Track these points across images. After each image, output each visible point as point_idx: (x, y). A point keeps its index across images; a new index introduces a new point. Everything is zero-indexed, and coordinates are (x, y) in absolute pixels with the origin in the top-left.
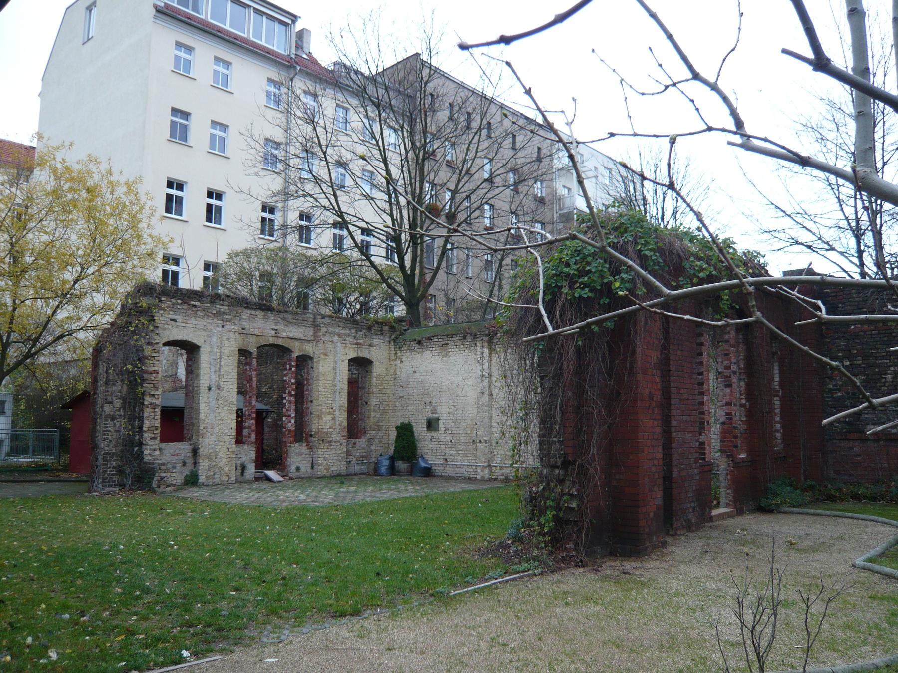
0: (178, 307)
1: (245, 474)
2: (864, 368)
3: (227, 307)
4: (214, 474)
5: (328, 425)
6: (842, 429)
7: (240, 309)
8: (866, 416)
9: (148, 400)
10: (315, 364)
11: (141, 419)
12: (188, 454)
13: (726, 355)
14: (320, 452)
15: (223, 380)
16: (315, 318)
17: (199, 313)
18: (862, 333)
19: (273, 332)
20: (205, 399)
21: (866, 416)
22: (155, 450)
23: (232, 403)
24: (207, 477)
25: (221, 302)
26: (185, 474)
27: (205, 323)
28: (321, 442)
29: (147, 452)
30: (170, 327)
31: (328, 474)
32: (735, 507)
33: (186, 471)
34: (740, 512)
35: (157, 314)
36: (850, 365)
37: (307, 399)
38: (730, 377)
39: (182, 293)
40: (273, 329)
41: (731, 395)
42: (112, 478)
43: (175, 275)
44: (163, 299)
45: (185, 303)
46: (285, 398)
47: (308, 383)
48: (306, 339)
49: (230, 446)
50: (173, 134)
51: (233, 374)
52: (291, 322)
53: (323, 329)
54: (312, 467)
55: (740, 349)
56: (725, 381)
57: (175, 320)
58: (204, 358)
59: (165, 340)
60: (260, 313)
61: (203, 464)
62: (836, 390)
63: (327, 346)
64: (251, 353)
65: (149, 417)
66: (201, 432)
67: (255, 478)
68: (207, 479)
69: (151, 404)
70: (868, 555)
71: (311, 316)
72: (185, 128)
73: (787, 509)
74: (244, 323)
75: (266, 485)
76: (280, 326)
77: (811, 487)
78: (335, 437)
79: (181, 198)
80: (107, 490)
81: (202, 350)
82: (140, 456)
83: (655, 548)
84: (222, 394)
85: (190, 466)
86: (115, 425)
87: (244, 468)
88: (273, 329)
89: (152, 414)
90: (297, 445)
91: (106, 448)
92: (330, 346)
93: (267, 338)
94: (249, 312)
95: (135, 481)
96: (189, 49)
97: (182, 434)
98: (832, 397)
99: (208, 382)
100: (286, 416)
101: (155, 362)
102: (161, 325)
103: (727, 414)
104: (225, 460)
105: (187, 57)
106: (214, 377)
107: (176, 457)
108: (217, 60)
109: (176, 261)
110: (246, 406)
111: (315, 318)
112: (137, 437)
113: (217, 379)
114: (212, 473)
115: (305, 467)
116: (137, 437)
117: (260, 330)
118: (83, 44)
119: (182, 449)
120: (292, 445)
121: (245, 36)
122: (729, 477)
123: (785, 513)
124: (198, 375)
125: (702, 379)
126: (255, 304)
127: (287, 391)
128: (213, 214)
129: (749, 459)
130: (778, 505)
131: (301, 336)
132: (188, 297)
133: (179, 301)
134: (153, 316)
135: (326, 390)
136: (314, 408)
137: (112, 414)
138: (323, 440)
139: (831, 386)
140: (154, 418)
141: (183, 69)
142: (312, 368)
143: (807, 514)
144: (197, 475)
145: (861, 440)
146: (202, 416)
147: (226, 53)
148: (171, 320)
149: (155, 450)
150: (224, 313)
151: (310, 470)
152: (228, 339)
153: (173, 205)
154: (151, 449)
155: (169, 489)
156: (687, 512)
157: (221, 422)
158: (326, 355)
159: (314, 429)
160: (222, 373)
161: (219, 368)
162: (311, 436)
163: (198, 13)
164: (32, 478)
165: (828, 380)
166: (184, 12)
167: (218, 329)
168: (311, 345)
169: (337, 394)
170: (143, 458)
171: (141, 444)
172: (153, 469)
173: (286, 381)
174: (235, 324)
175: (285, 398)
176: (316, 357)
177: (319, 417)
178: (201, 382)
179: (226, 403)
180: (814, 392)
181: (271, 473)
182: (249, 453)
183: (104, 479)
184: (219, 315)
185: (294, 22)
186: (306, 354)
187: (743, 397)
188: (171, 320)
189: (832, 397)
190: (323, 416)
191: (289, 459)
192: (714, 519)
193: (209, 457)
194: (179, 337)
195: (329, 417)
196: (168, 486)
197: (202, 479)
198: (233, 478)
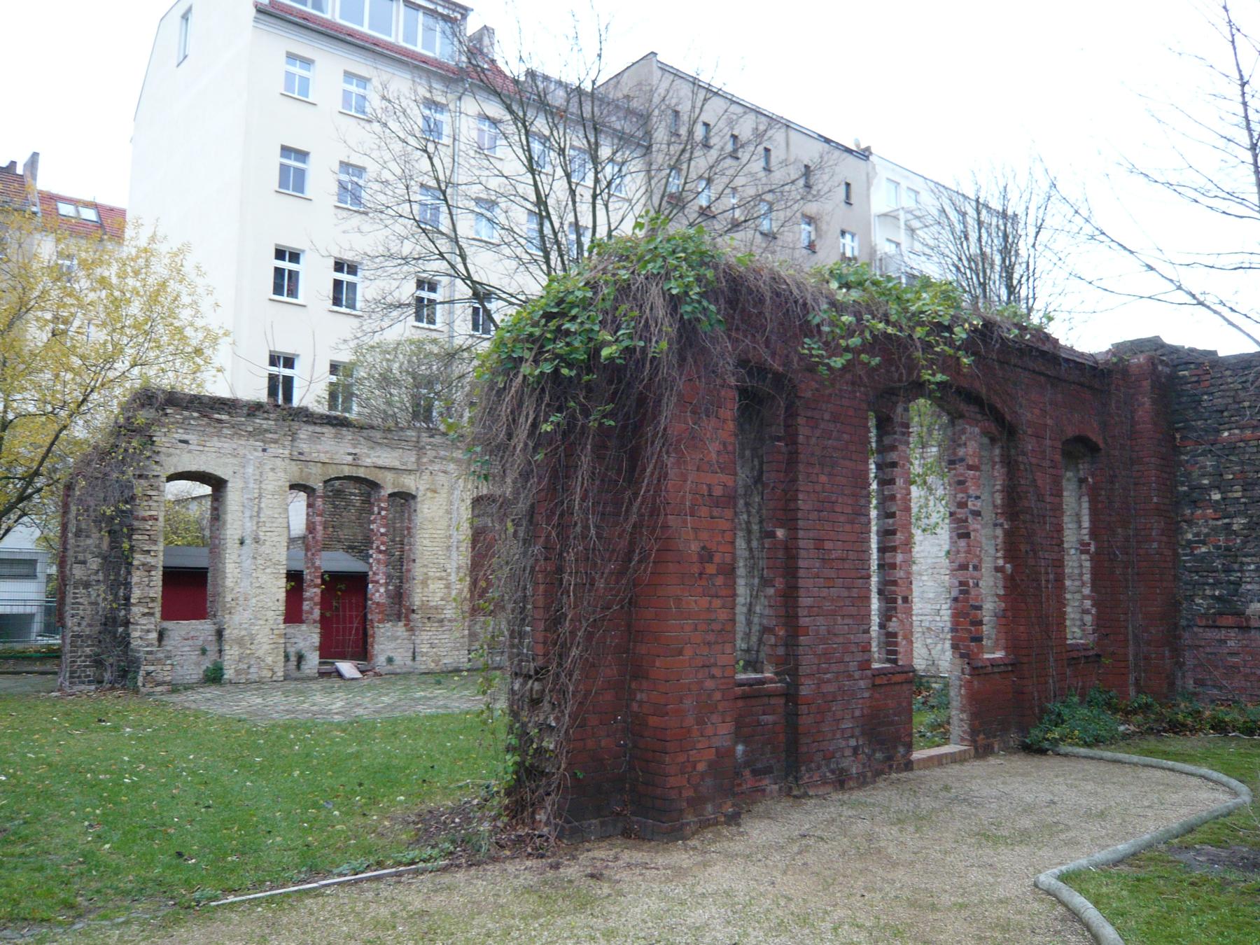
0: (192, 422)
1: (302, 667)
2: (1245, 504)
3: (273, 423)
4: (249, 668)
5: (439, 595)
6: (1208, 609)
7: (295, 425)
8: (1249, 587)
9: (138, 559)
10: (419, 506)
11: (127, 585)
12: (210, 638)
13: (961, 483)
14: (425, 636)
15: (264, 529)
16: (419, 437)
17: (225, 431)
18: (1242, 444)
20: (234, 557)
21: (1249, 587)
22: (148, 631)
23: (278, 563)
24: (238, 672)
25: (265, 415)
26: (204, 667)
27: (235, 446)
28: (426, 621)
29: (136, 634)
30: (178, 451)
31: (437, 669)
32: (974, 742)
33: (207, 663)
34: (982, 751)
35: (158, 434)
36: (1224, 499)
37: (409, 556)
38: (966, 521)
39: (201, 403)
40: (350, 454)
41: (968, 552)
42: (85, 671)
44: (169, 411)
45: (205, 416)
46: (371, 556)
47: (409, 533)
48: (404, 467)
49: (275, 627)
50: (283, 183)
51: (280, 520)
52: (379, 443)
53: (431, 454)
54: (414, 659)
56: (958, 528)
57: (186, 442)
58: (233, 497)
59: (172, 471)
60: (329, 431)
61: (232, 652)
62: (1196, 542)
64: (314, 490)
65: (140, 583)
66: (228, 605)
67: (319, 673)
68: (237, 675)
69: (144, 565)
70: (1064, 868)
72: (301, 174)
73: (1069, 749)
74: (301, 445)
75: (337, 682)
76: (362, 450)
77: (1146, 708)
78: (449, 613)
79: (297, 273)
80: (76, 688)
81: (229, 485)
82: (125, 641)
83: (705, 824)
84: (262, 549)
85: (212, 655)
86: (89, 595)
87: (300, 658)
88: (350, 454)
89: (146, 579)
90: (389, 625)
91: (76, 628)
92: (442, 478)
93: (339, 467)
94: (311, 428)
95: (119, 676)
96: (307, 62)
97: (205, 609)
98: (1192, 554)
99: (240, 532)
100: (373, 582)
101: (151, 503)
102: (163, 450)
103: (961, 584)
104: (266, 647)
105: (304, 73)
106: (248, 524)
107: (190, 642)
108: (349, 75)
109: (289, 362)
110: (308, 568)
111: (419, 437)
112: (123, 613)
113: (255, 528)
114: (245, 666)
115: (402, 659)
116: (123, 613)
117: (328, 456)
118: (178, 65)
119: (203, 629)
120: (381, 626)
121: (391, 39)
122: (963, 692)
123: (1066, 755)
124: (224, 523)
125: (894, 524)
126: (322, 416)
127: (374, 546)
128: (341, 294)
130: (1055, 742)
131: (396, 464)
132: (212, 408)
133: (195, 414)
134: (151, 437)
135: (434, 544)
136: (418, 571)
137: (85, 578)
138: (429, 618)
139: (1190, 536)
140: (148, 585)
141: (297, 91)
142: (415, 511)
143: (1101, 759)
144: (221, 669)
145: (1240, 628)
146: (229, 582)
147: (360, 65)
148: (181, 441)
149: (148, 631)
150: (266, 431)
151: (409, 663)
152: (273, 469)
153: (285, 283)
154: (142, 630)
155: (159, 689)
156: (838, 755)
157: (261, 591)
158: (435, 492)
159: (417, 600)
160: (262, 520)
161: (258, 513)
162: (413, 611)
163: (321, 10)
164: (29, 669)
165: (1185, 526)
166: (301, 10)
167: (256, 454)
168: (412, 477)
169: (455, 549)
170: (129, 643)
171: (127, 623)
172: (138, 658)
173: (372, 530)
174: (284, 447)
175: (371, 556)
176: (420, 494)
177: (424, 583)
178: (229, 532)
179: (269, 563)
180: (1155, 545)
181: (347, 668)
182: (308, 637)
183: (72, 672)
184: (257, 433)
185: (464, 17)
186: (404, 490)
187: (999, 554)
188: (181, 441)
189: (1192, 554)
190: (429, 582)
191: (376, 646)
192: (915, 766)
193: (240, 642)
194: (194, 468)
195: (441, 584)
196: (158, 685)
197: (229, 674)
198: (280, 674)
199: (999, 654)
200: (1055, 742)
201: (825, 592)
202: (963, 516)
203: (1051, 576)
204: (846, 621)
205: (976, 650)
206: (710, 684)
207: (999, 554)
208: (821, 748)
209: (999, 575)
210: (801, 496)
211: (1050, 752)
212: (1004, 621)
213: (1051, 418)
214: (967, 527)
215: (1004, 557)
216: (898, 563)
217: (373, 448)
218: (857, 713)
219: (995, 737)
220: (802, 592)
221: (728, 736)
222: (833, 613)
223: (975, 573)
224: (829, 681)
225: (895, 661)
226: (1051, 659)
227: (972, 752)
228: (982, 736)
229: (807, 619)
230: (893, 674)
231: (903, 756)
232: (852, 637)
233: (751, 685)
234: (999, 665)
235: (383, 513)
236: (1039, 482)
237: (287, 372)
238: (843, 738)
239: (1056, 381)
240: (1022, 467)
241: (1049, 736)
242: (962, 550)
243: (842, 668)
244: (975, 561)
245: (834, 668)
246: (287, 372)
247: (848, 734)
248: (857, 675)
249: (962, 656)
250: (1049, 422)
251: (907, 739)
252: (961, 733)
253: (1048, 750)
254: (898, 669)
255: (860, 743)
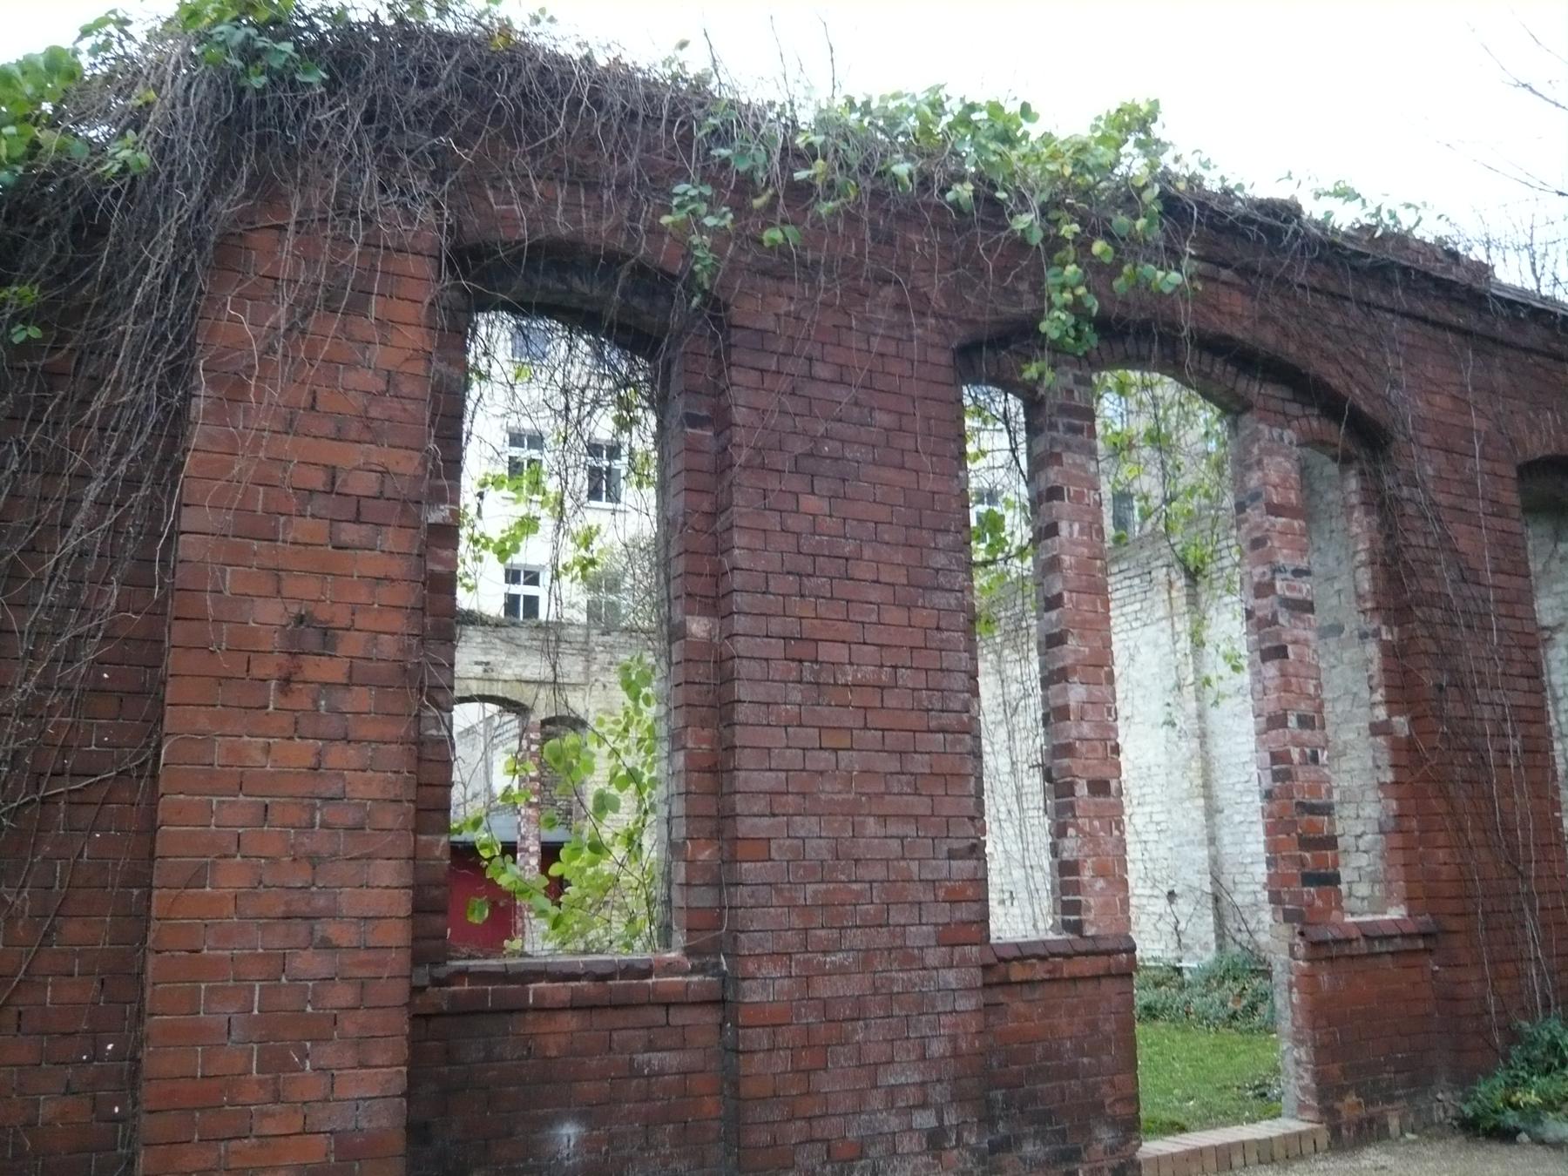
16: (588, 636)
19: (479, 670)
32: (1328, 1113)
38: (1274, 621)
40: (477, 663)
43: (532, 602)
55: (1355, 529)
63: (613, 693)
71: (580, 632)
88: (477, 663)
122: (1295, 998)
129: (1410, 928)
168: (579, 694)
199: (1396, 913)
200: (1534, 1115)
201: (824, 760)
202: (1268, 612)
203: (1514, 743)
204: (893, 829)
205: (1319, 903)
206: (309, 963)
207: (1378, 696)
208: (818, 1134)
209: (1380, 740)
210: (739, 539)
211: (1523, 1137)
212: (1398, 840)
213: (1481, 414)
214: (1278, 636)
215: (1388, 702)
216: (1073, 704)
217: (514, 654)
218: (937, 1048)
219: (1390, 1099)
220: (744, 758)
221: (378, 1105)
222: (852, 812)
223: (1306, 734)
224: (841, 970)
225: (1076, 928)
226: (1529, 923)
227: (1324, 1138)
228: (1351, 1099)
229: (766, 821)
230: (1067, 956)
231: (1112, 1150)
232: (914, 866)
233: (602, 978)
234: (1390, 938)
235: (534, 748)
236: (1463, 545)
237: (531, 590)
238: (890, 1106)
239: (1485, 343)
240: (1410, 509)
241: (1520, 1097)
242: (1270, 684)
243: (882, 938)
244: (1305, 707)
245: (857, 938)
246: (531, 590)
247: (912, 1096)
248: (933, 956)
249: (1289, 917)
250: (1476, 422)
251: (1120, 1110)
252: (1298, 1093)
253: (1518, 1131)
254: (1082, 946)
255: (950, 1119)
